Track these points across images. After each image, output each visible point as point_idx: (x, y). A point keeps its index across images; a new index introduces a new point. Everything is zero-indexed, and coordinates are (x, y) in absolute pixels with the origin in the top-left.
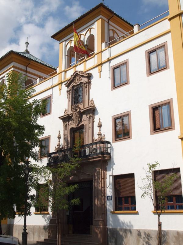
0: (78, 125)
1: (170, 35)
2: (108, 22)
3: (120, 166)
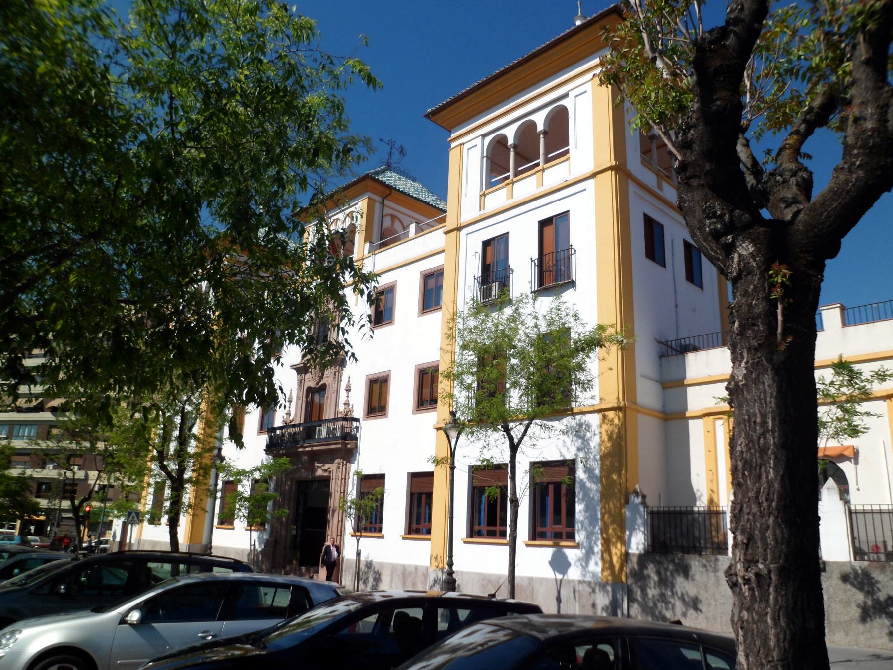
0: (317, 384)
1: (443, 254)
2: (383, 204)
3: (366, 462)
